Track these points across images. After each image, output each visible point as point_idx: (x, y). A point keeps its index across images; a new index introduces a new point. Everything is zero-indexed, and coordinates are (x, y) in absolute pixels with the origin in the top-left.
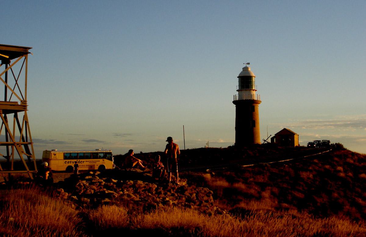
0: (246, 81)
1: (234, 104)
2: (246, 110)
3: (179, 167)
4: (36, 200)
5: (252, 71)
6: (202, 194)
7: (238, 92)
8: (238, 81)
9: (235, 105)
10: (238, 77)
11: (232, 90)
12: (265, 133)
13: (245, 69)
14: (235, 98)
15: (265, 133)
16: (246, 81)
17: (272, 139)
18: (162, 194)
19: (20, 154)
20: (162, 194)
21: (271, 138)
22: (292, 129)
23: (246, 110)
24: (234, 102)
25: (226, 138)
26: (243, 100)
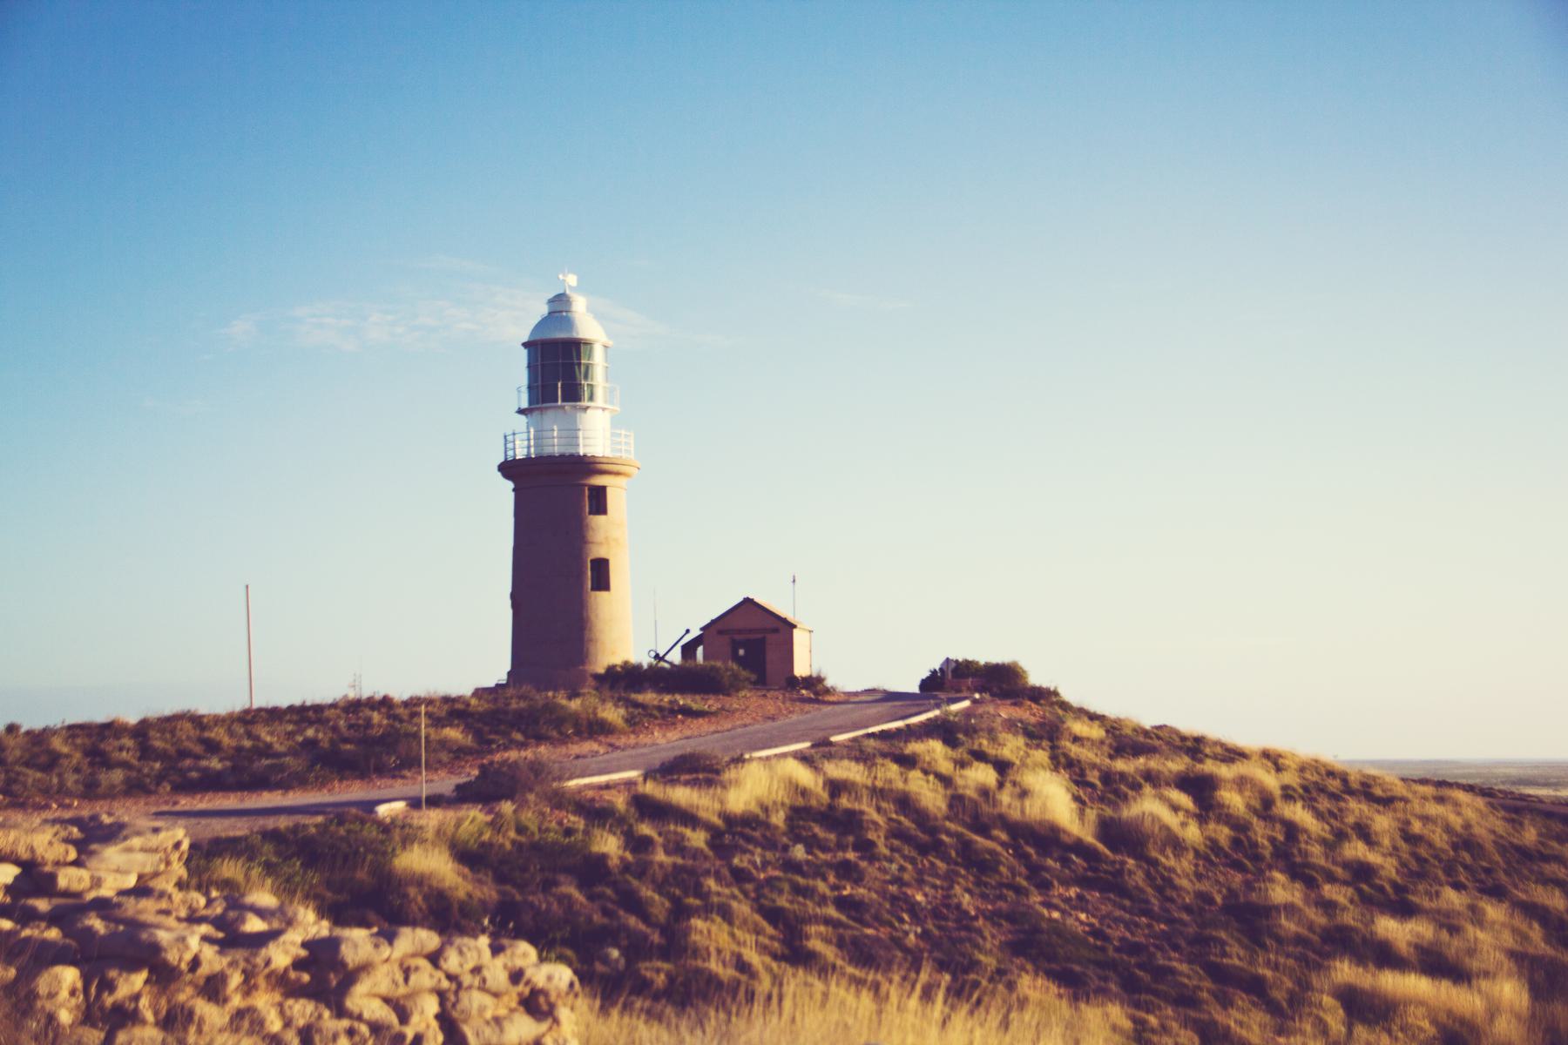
0: (557, 368)
1: (507, 476)
2: (556, 505)
3: (295, 788)
4: (1062, 905)
5: (587, 324)
6: (488, 1000)
7: (523, 418)
8: (525, 362)
9: (510, 485)
10: (525, 345)
11: (503, 423)
12: (640, 621)
13: (559, 306)
14: (510, 446)
15: (640, 621)
16: (557, 368)
17: (688, 650)
18: (143, 1022)
19: (193, 821)
20: (143, 1022)
21: (684, 647)
22: (779, 606)
23: (556, 505)
24: (509, 469)
25: (470, 650)
26: (551, 458)
